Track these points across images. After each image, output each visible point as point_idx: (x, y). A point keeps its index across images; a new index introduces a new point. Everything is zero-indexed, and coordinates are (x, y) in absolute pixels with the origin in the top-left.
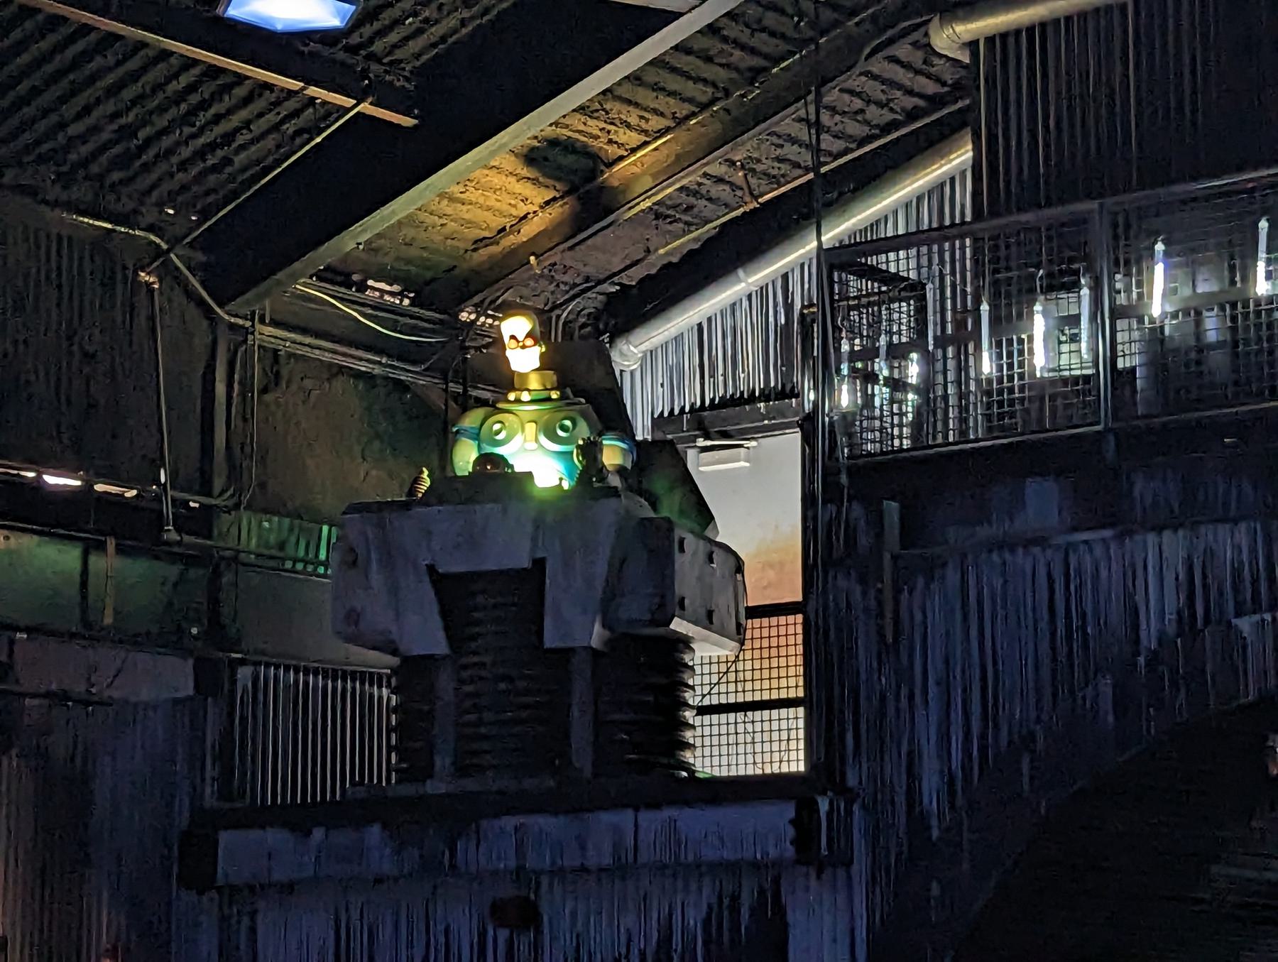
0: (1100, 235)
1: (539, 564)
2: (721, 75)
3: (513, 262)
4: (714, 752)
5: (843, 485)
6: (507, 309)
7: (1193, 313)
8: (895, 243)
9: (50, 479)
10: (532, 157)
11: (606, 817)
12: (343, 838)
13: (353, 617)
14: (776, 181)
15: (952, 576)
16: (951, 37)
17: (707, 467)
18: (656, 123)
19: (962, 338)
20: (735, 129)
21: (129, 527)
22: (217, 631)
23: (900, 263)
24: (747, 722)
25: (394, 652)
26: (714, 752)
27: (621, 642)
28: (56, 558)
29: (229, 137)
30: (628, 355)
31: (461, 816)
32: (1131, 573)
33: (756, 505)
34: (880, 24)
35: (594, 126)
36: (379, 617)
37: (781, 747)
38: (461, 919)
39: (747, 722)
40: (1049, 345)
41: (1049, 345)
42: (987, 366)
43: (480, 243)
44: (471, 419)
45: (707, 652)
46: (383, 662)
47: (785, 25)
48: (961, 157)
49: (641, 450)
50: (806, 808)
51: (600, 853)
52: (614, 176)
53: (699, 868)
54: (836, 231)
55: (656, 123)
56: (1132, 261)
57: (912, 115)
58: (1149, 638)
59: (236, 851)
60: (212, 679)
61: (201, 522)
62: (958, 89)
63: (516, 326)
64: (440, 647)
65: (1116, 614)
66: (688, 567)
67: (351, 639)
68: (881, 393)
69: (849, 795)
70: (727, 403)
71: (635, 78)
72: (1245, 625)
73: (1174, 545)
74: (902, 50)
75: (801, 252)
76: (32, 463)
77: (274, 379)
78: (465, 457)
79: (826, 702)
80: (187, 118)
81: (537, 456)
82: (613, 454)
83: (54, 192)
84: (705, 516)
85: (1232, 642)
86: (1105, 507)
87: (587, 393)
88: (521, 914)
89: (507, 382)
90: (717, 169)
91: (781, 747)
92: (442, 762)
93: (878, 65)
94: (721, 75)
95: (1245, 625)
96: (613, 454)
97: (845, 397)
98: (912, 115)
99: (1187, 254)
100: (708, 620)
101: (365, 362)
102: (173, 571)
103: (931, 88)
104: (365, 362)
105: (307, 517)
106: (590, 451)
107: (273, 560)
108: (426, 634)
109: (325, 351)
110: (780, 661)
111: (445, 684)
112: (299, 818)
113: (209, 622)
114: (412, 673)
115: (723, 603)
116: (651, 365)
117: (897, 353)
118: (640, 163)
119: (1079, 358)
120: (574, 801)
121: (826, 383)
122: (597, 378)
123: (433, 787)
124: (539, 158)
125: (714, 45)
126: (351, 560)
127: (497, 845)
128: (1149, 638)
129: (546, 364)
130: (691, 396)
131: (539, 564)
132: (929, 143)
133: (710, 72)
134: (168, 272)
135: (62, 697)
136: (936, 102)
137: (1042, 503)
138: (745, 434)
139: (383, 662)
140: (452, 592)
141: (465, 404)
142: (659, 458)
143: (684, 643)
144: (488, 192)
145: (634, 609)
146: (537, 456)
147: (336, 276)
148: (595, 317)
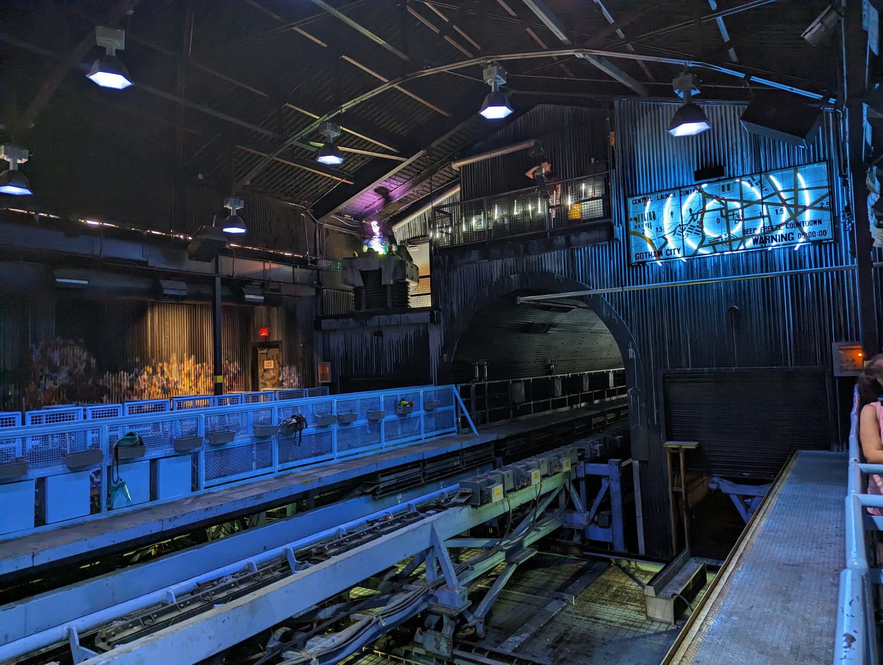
0: (485, 203)
1: (380, 269)
2: (412, 174)
3: (373, 211)
4: (414, 303)
5: (437, 253)
6: (372, 220)
7: (502, 218)
8: (445, 206)
9: (89, 222)
10: (376, 190)
11: (395, 316)
12: (345, 320)
13: (346, 279)
14: (422, 195)
15: (458, 269)
16: (456, 166)
17: (412, 250)
18: (399, 183)
19: (459, 224)
20: (414, 185)
21: (302, 263)
22: (319, 283)
23: (446, 210)
24: (420, 297)
25: (353, 285)
26: (414, 303)
27: (397, 283)
28: (288, 269)
29: (317, 187)
30: (396, 229)
31: (370, 315)
32: (491, 268)
33: (421, 257)
34: (442, 164)
35: (388, 184)
36: (350, 279)
37: (427, 302)
38: (368, 335)
39: (420, 297)
40: (476, 223)
41: (476, 223)
42: (464, 229)
43: (366, 207)
44: (366, 241)
45: (412, 285)
46: (351, 288)
47: (424, 164)
48: (458, 189)
49: (399, 247)
50: (432, 313)
51: (394, 322)
52: (391, 194)
53: (412, 324)
54: (435, 204)
55: (399, 183)
56: (491, 208)
57: (448, 181)
58: (495, 279)
59: (325, 324)
60: (318, 291)
61: (315, 262)
62: (457, 176)
63: (374, 223)
64: (362, 284)
65: (489, 274)
66: (408, 269)
67: (345, 284)
68: (444, 235)
69: (440, 310)
70: (414, 238)
71: (395, 174)
72: (512, 276)
73: (499, 262)
74: (446, 169)
75: (429, 207)
76: (282, 251)
77: (327, 235)
78: (365, 249)
79: (434, 294)
80: (309, 183)
81: (378, 246)
82: (394, 249)
83: (283, 198)
84: (411, 260)
85: (510, 279)
86: (486, 255)
87: (388, 236)
88: (379, 334)
89: (373, 234)
90: (411, 192)
91: (427, 302)
92: (364, 306)
93: (442, 172)
94: (412, 174)
95: (512, 276)
96: (394, 249)
97: (438, 235)
98: (448, 181)
99: (502, 207)
100: (412, 279)
101: (344, 231)
102: (310, 271)
103: (451, 176)
104: (344, 231)
105: (335, 261)
106: (390, 248)
107: (328, 270)
108: (360, 283)
109: (337, 229)
110: (426, 286)
111: (363, 292)
112: (337, 317)
113: (318, 282)
114: (357, 290)
115: (415, 276)
116: (400, 230)
117: (447, 227)
118: (397, 191)
119: (482, 226)
120: (388, 313)
121: (435, 232)
122: (390, 233)
123: (362, 311)
124: (378, 191)
125: (410, 168)
126: (344, 268)
127: (375, 321)
128: (495, 279)
129: (380, 231)
130: (407, 237)
131: (380, 269)
132: (451, 187)
133: (410, 173)
134: (306, 213)
135: (290, 296)
136: (452, 179)
137: (475, 255)
138: (418, 244)
139: (351, 288)
140: (364, 274)
141: (364, 239)
142: (402, 248)
143: (408, 283)
144: (367, 198)
145: (398, 277)
146: (378, 246)
147: (339, 214)
148: (388, 222)
